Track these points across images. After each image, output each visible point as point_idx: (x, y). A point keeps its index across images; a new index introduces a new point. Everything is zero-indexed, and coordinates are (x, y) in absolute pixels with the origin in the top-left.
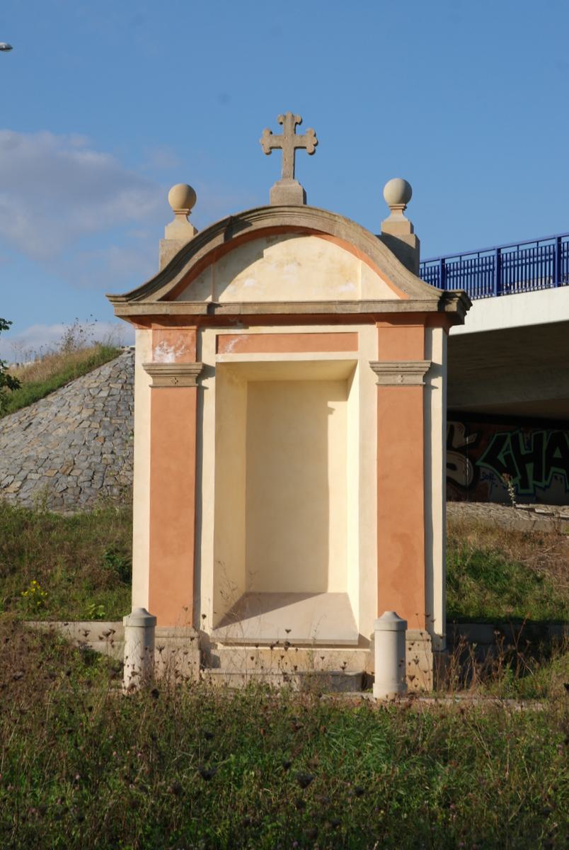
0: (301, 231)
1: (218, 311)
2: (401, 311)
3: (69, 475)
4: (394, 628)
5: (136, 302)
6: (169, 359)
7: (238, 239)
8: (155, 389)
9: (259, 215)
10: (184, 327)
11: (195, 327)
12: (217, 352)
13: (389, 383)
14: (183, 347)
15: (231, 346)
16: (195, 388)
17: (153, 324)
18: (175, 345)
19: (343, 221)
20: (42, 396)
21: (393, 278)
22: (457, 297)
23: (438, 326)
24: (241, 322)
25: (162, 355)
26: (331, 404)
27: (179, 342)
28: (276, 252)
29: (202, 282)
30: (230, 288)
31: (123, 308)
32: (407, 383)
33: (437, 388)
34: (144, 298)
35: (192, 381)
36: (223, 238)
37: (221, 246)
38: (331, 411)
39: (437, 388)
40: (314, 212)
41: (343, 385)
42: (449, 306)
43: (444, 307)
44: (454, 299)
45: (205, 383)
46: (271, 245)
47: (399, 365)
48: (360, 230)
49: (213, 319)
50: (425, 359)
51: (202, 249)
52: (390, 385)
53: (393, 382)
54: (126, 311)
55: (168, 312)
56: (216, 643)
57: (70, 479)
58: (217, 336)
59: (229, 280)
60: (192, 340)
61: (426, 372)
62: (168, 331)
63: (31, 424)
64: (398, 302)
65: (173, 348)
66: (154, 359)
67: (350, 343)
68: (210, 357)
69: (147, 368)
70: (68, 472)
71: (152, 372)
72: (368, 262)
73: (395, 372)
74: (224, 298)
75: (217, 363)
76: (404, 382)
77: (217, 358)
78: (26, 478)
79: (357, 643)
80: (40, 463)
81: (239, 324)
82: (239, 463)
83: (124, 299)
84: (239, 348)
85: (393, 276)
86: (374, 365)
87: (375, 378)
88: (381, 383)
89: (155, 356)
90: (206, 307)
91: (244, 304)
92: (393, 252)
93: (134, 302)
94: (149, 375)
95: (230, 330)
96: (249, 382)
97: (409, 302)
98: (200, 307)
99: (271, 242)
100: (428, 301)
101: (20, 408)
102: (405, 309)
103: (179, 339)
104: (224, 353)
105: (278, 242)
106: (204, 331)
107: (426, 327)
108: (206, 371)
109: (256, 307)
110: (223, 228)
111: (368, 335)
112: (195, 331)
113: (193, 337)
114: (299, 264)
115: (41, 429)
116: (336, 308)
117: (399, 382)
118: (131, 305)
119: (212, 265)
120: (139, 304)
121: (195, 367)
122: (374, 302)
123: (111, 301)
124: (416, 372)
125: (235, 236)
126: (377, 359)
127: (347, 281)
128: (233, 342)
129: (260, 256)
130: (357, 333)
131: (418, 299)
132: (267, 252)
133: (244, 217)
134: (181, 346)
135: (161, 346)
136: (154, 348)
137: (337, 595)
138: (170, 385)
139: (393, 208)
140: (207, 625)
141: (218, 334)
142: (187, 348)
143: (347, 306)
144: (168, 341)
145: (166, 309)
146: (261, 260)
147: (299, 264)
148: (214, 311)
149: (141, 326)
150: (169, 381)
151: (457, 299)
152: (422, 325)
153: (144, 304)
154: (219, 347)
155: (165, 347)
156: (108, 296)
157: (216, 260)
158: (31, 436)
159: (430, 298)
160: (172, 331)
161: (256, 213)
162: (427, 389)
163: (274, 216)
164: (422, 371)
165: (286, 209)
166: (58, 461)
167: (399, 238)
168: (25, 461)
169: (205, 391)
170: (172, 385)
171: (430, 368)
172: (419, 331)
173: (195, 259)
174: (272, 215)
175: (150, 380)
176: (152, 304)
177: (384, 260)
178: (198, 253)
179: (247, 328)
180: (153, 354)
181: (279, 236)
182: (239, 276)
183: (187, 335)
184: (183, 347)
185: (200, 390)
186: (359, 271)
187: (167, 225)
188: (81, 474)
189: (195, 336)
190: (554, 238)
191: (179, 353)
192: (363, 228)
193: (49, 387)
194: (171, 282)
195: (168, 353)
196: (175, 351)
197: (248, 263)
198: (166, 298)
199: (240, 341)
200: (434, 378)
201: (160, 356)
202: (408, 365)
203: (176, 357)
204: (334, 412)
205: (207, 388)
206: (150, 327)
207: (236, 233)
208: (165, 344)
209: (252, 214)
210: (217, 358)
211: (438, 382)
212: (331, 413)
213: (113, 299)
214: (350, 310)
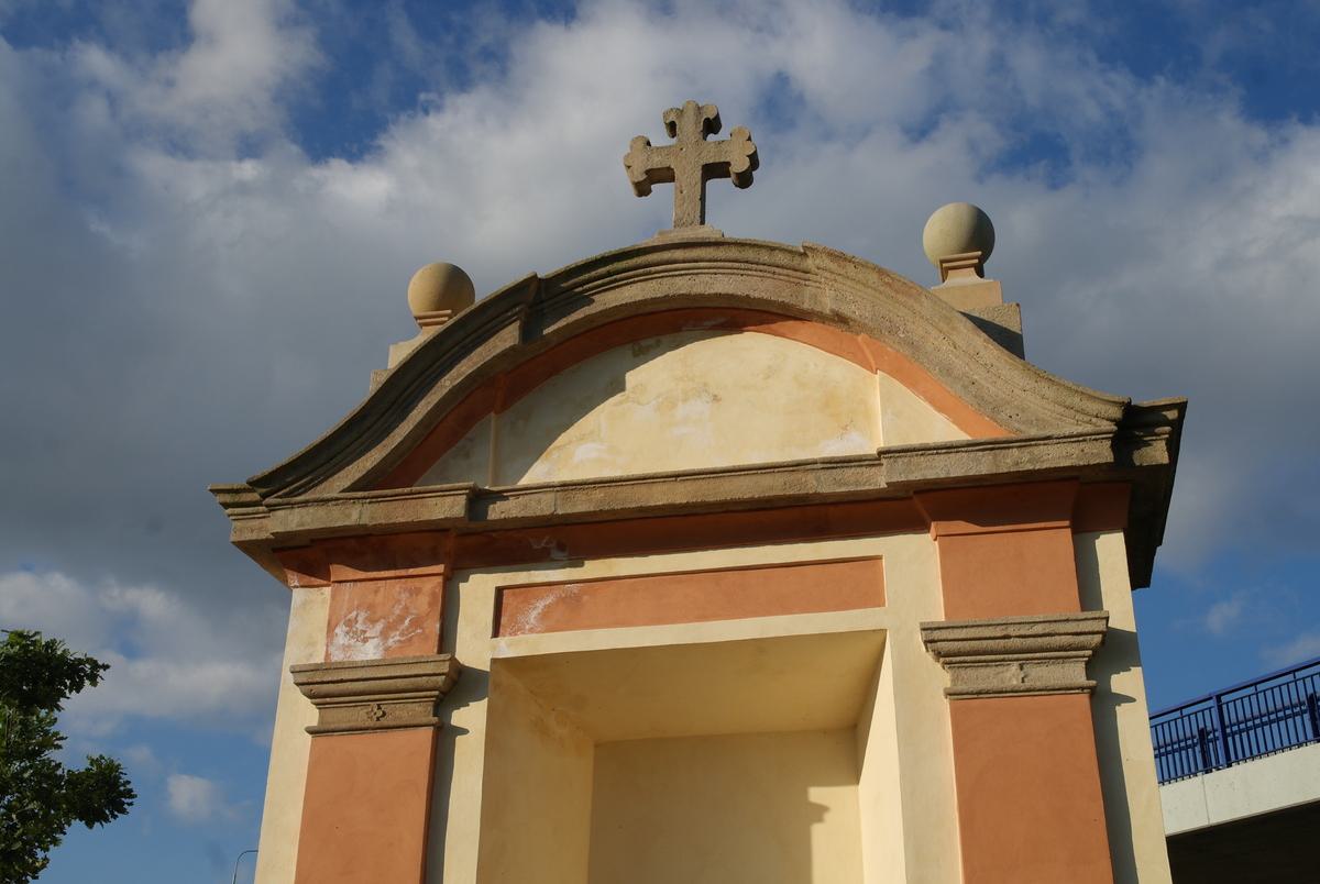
1: (497, 511)
5: (286, 500)
6: (370, 651)
8: (323, 740)
10: (412, 571)
11: (440, 568)
12: (496, 634)
14: (407, 622)
15: (534, 614)
16: (429, 731)
19: (827, 262)
21: (973, 389)
24: (561, 547)
25: (349, 646)
26: (817, 794)
28: (656, 378)
29: (467, 456)
31: (256, 523)
32: (1039, 684)
33: (1132, 700)
34: (306, 488)
35: (422, 711)
36: (517, 333)
37: (512, 348)
38: (819, 812)
39: (1132, 700)
40: (750, 254)
41: (844, 742)
42: (1146, 450)
44: (1158, 430)
45: (459, 717)
47: (1011, 631)
48: (873, 277)
50: (1083, 609)
51: (464, 361)
53: (995, 684)
54: (260, 529)
55: (365, 520)
58: (500, 591)
60: (431, 605)
61: (1095, 650)
65: (379, 626)
66: (327, 655)
67: (864, 585)
68: (476, 647)
69: (303, 678)
72: (897, 372)
75: (494, 661)
77: (494, 648)
79: (505, 592)
81: (556, 554)
83: (255, 496)
84: (550, 623)
86: (937, 635)
87: (942, 678)
88: (961, 687)
89: (332, 649)
90: (462, 500)
91: (565, 486)
97: (1027, 442)
98: (449, 500)
99: (643, 354)
103: (399, 601)
106: (466, 580)
107: (1077, 530)
108: (460, 685)
109: (598, 494)
111: (913, 570)
112: (440, 579)
113: (433, 594)
114: (716, 398)
116: (818, 479)
118: (272, 508)
120: (292, 505)
121: (429, 669)
123: (226, 505)
124: (1062, 653)
125: (546, 332)
126: (939, 616)
127: (845, 428)
128: (541, 605)
129: (618, 386)
130: (878, 558)
132: (632, 378)
134: (401, 619)
135: (350, 623)
137: (329, 570)
138: (360, 724)
139: (946, 267)
142: (416, 623)
143: (849, 473)
144: (371, 607)
145: (358, 515)
146: (618, 397)
147: (716, 398)
149: (308, 579)
150: (359, 716)
151: (1167, 429)
152: (1067, 523)
153: (306, 503)
154: (504, 620)
155: (360, 626)
157: (505, 405)
159: (1089, 428)
160: (380, 583)
164: (1084, 657)
165: (678, 254)
169: (459, 739)
170: (369, 723)
172: (1055, 541)
174: (645, 273)
175: (311, 715)
177: (945, 346)
178: (454, 372)
181: (665, 339)
182: (562, 439)
183: (418, 591)
184: (407, 622)
185: (444, 737)
186: (876, 401)
187: (396, 343)
189: (439, 591)
190: (1211, 698)
191: (395, 638)
192: (881, 272)
195: (365, 640)
196: (384, 635)
199: (562, 600)
201: (346, 648)
202: (1038, 629)
203: (387, 649)
204: (828, 816)
205: (464, 731)
206: (325, 575)
210: (494, 648)
212: (820, 820)
213: (228, 498)
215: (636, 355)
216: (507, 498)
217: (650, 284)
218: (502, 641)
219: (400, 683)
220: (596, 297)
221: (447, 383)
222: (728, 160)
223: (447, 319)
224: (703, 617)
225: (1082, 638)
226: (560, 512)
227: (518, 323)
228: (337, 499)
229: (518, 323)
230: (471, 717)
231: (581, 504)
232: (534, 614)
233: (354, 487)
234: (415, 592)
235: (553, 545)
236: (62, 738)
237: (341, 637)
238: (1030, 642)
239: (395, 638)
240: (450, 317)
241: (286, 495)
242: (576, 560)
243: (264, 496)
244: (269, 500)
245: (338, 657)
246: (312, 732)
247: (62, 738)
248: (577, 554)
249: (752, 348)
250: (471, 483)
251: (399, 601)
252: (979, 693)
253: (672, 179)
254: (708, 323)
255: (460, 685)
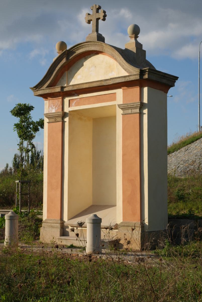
0: (95, 53)
1: (65, 89)
2: (126, 81)
3: (192, 165)
4: (91, 222)
6: (54, 111)
7: (72, 57)
8: (49, 124)
9: (77, 48)
10: (58, 98)
11: (61, 97)
12: (69, 107)
13: (126, 113)
15: (74, 104)
17: (48, 98)
18: (55, 105)
20: (195, 140)
21: (123, 67)
22: (147, 72)
23: (146, 86)
24: (76, 93)
27: (57, 104)
28: (89, 63)
29: (63, 79)
30: (73, 80)
31: (36, 93)
33: (146, 114)
34: (41, 87)
35: (60, 119)
39: (146, 114)
43: (143, 77)
44: (146, 73)
46: (86, 60)
47: (129, 105)
49: (64, 94)
51: (59, 65)
52: (128, 114)
53: (128, 113)
56: (69, 226)
57: (192, 166)
58: (69, 100)
59: (72, 77)
62: (53, 100)
63: (188, 149)
64: (128, 76)
65: (55, 107)
68: (67, 110)
69: (45, 115)
70: (192, 164)
71: (47, 117)
73: (128, 108)
74: (71, 84)
75: (69, 111)
76: (132, 112)
78: (179, 167)
80: (185, 162)
81: (75, 94)
82: (87, 151)
84: (77, 105)
85: (123, 66)
86: (120, 106)
88: (124, 114)
90: (60, 88)
92: (121, 55)
93: (38, 90)
94: (47, 118)
95: (73, 97)
96: (93, 119)
98: (58, 89)
99: (86, 59)
100: (135, 75)
101: (187, 145)
102: (127, 80)
104: (71, 107)
105: (88, 59)
106: (65, 99)
108: (64, 115)
109: (77, 86)
110: (65, 56)
111: (119, 92)
112: (61, 99)
115: (190, 151)
117: (130, 112)
118: (37, 91)
119: (66, 72)
120: (40, 90)
122: (116, 78)
124: (136, 108)
125: (70, 58)
126: (122, 103)
127: (112, 71)
128: (75, 102)
129: (83, 65)
130: (116, 93)
131: (131, 74)
132: (85, 63)
133: (74, 50)
135: (51, 106)
136: (49, 107)
138: (53, 122)
140: (65, 219)
141: (70, 99)
143: (108, 81)
144: (53, 104)
148: (64, 90)
151: (147, 72)
152: (139, 86)
153: (41, 90)
154: (70, 105)
155: (52, 107)
156: (31, 88)
158: (186, 153)
161: (76, 47)
162: (141, 114)
163: (83, 48)
165: (86, 44)
166: (190, 161)
167: (130, 49)
168: (181, 161)
169: (66, 123)
171: (140, 105)
172: (137, 90)
173: (58, 68)
174: (82, 47)
176: (43, 89)
179: (78, 95)
180: (49, 110)
182: (76, 74)
185: (63, 123)
188: (196, 165)
189: (61, 101)
193: (198, 138)
194: (49, 80)
195: (53, 109)
196: (55, 108)
197: (78, 69)
198: (49, 86)
200: (144, 110)
201: (51, 110)
202: (132, 105)
203: (56, 110)
205: (66, 122)
207: (71, 57)
208: (53, 105)
209: (75, 48)
211: (145, 111)
214: (109, 83)
215: (85, 59)
216: (66, 87)
217: (83, 49)
218: (70, 108)
219: (57, 116)
220: (76, 52)
221: (57, 69)
222: (100, 17)
223: (61, 52)
224: (94, 103)
225: (137, 106)
226: (73, 89)
227: (65, 58)
228: (45, 89)
229: (65, 58)
230: (67, 119)
231: (75, 88)
232: (74, 104)
233: (47, 87)
234: (58, 101)
235: (75, 93)
236: (32, 117)
237: (50, 109)
238: (131, 106)
239: (57, 108)
240: (62, 52)
241: (39, 89)
242: (78, 95)
243: (36, 89)
244: (37, 90)
245: (50, 112)
246: (48, 123)
247: (32, 117)
248: (78, 95)
249: (100, 56)
250: (60, 86)
251: (57, 103)
252: (125, 114)
253: (92, 21)
254: (94, 53)
255: (64, 115)
